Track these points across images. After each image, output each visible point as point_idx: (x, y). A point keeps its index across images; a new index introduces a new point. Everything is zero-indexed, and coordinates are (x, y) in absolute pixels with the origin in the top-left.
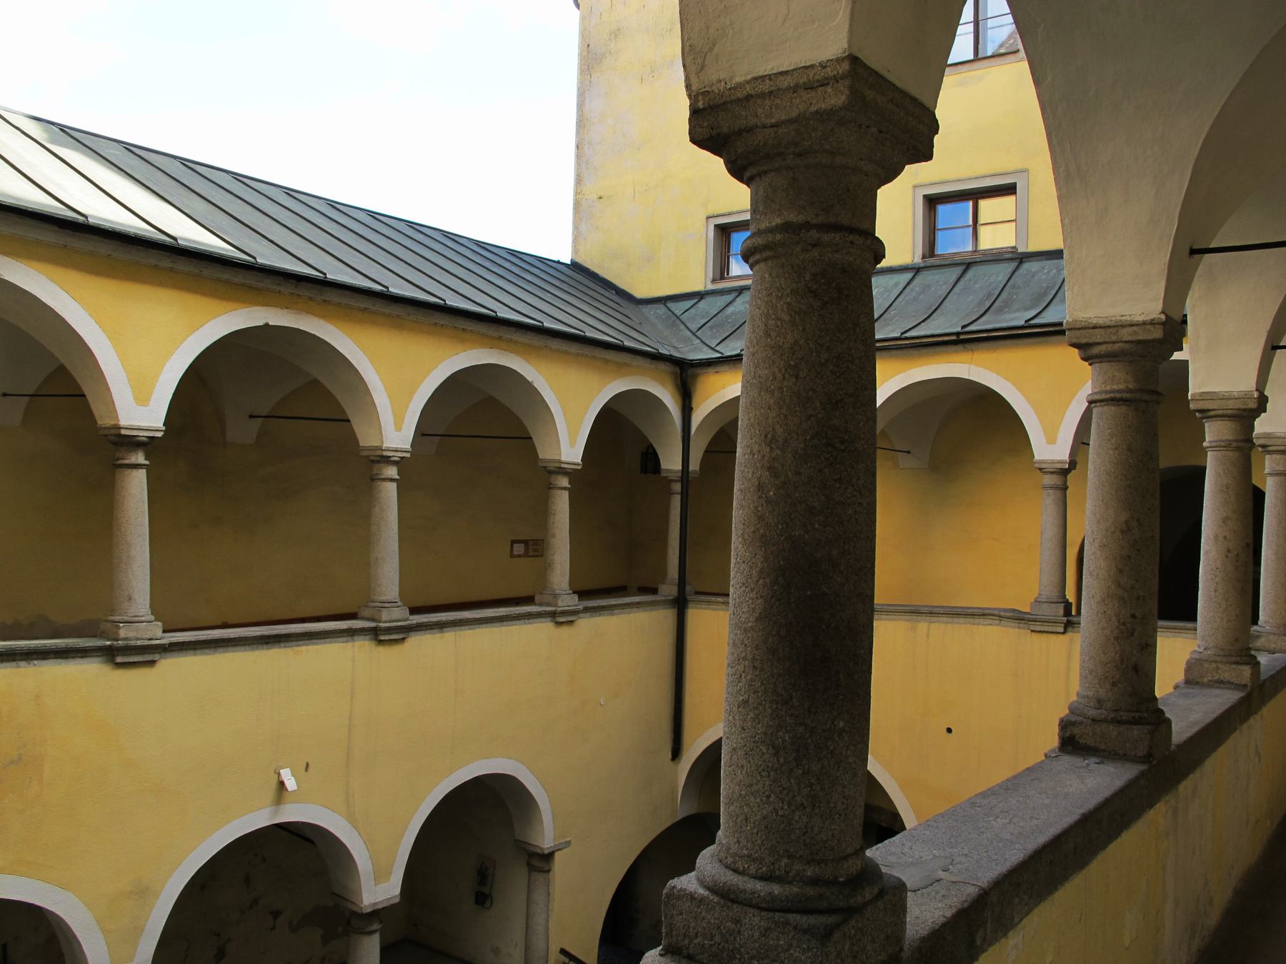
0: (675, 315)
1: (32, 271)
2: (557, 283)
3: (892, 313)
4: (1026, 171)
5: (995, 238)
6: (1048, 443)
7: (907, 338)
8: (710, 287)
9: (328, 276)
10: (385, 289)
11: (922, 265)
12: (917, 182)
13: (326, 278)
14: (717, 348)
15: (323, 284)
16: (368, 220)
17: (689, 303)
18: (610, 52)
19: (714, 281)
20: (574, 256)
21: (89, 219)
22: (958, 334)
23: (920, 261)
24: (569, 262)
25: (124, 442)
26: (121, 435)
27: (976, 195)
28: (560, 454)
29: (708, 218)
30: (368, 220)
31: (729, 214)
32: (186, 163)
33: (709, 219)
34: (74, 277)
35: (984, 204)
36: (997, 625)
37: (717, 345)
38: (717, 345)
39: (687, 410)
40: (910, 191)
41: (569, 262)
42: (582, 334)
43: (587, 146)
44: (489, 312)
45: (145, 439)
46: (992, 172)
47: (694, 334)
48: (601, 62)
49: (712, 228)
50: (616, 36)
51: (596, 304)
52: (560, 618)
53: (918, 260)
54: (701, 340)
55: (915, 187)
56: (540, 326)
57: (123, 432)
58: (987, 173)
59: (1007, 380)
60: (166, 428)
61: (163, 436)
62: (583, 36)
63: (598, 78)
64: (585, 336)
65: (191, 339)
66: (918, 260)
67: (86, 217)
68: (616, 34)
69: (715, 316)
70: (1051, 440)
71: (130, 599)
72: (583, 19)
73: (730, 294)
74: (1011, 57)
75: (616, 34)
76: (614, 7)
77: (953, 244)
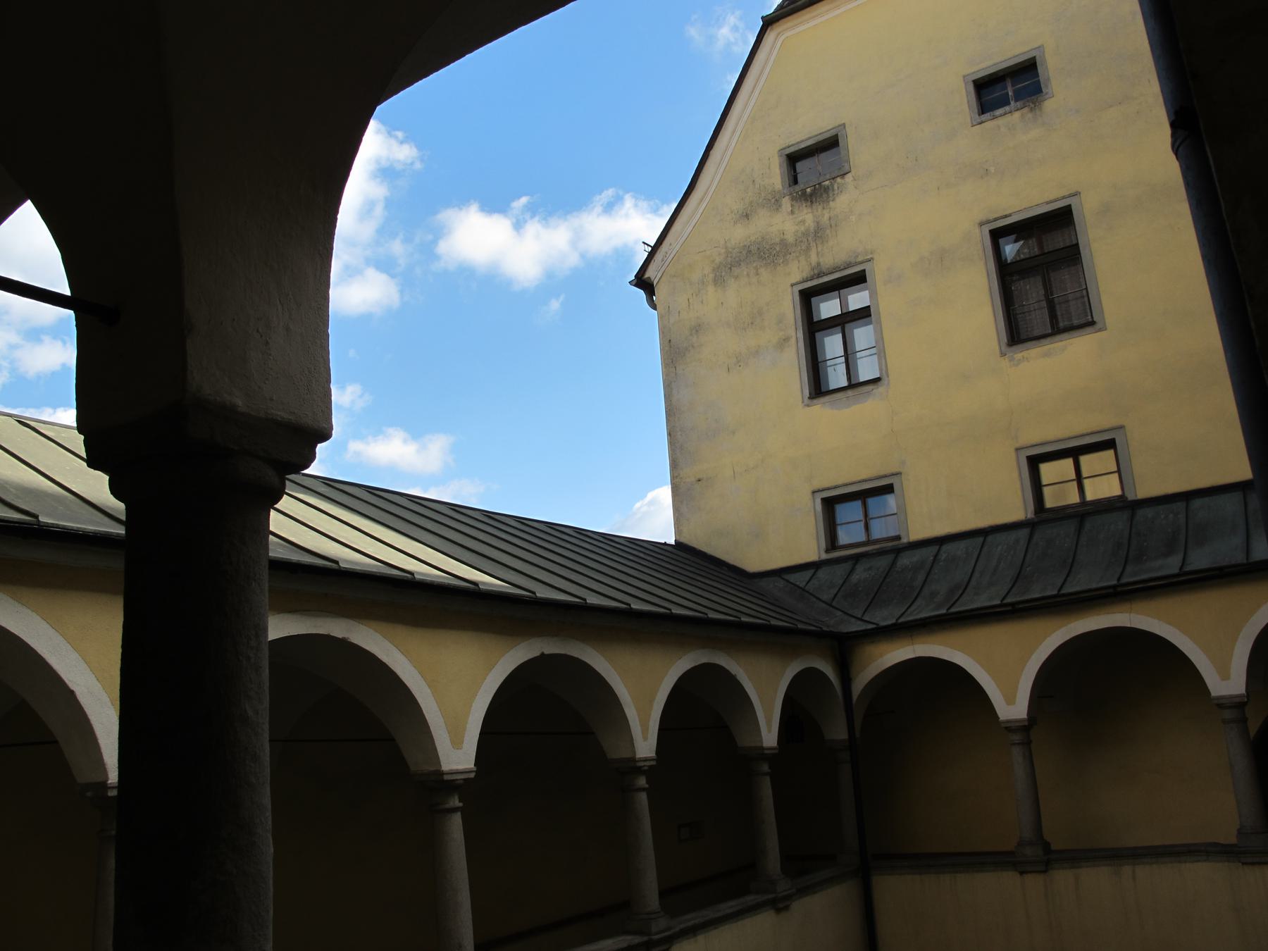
0: (801, 588)
1: (371, 631)
2: (654, 567)
3: (1028, 569)
4: (1122, 427)
5: (1102, 488)
6: (1223, 680)
7: (1064, 595)
8: (824, 556)
9: (588, 601)
10: (668, 611)
11: (1036, 520)
12: (1018, 445)
13: (586, 603)
14: (866, 618)
15: (583, 609)
16: (651, 548)
17: (810, 573)
18: (693, 347)
19: (827, 551)
20: (678, 538)
21: (340, 564)
22: (1114, 587)
23: (1033, 516)
24: (673, 543)
25: (440, 784)
26: (443, 781)
27: (1074, 453)
28: (761, 741)
29: (814, 492)
30: (602, 539)
31: (836, 487)
32: (412, 499)
33: (815, 494)
34: (401, 631)
35: (1085, 460)
36: (1205, 861)
37: (864, 613)
38: (864, 613)
39: (846, 680)
40: (1013, 454)
41: (673, 543)
42: (706, 616)
43: (679, 433)
44: (330, 564)
45: (462, 782)
46: (1089, 431)
47: (831, 605)
48: (684, 355)
49: (818, 502)
50: (697, 331)
51: (730, 584)
52: (779, 905)
53: (1030, 515)
54: (842, 611)
55: (1017, 450)
56: (766, 624)
57: (446, 777)
58: (1085, 432)
59: (1170, 624)
60: (477, 769)
61: (475, 776)
62: (663, 333)
63: (684, 370)
64: (770, 625)
65: (489, 679)
66: (1030, 515)
67: (336, 562)
68: (697, 329)
69: (842, 585)
70: (1225, 675)
71: (460, 947)
72: (661, 318)
73: (846, 562)
74: (1089, 329)
75: (697, 329)
76: (691, 307)
77: (1060, 495)
